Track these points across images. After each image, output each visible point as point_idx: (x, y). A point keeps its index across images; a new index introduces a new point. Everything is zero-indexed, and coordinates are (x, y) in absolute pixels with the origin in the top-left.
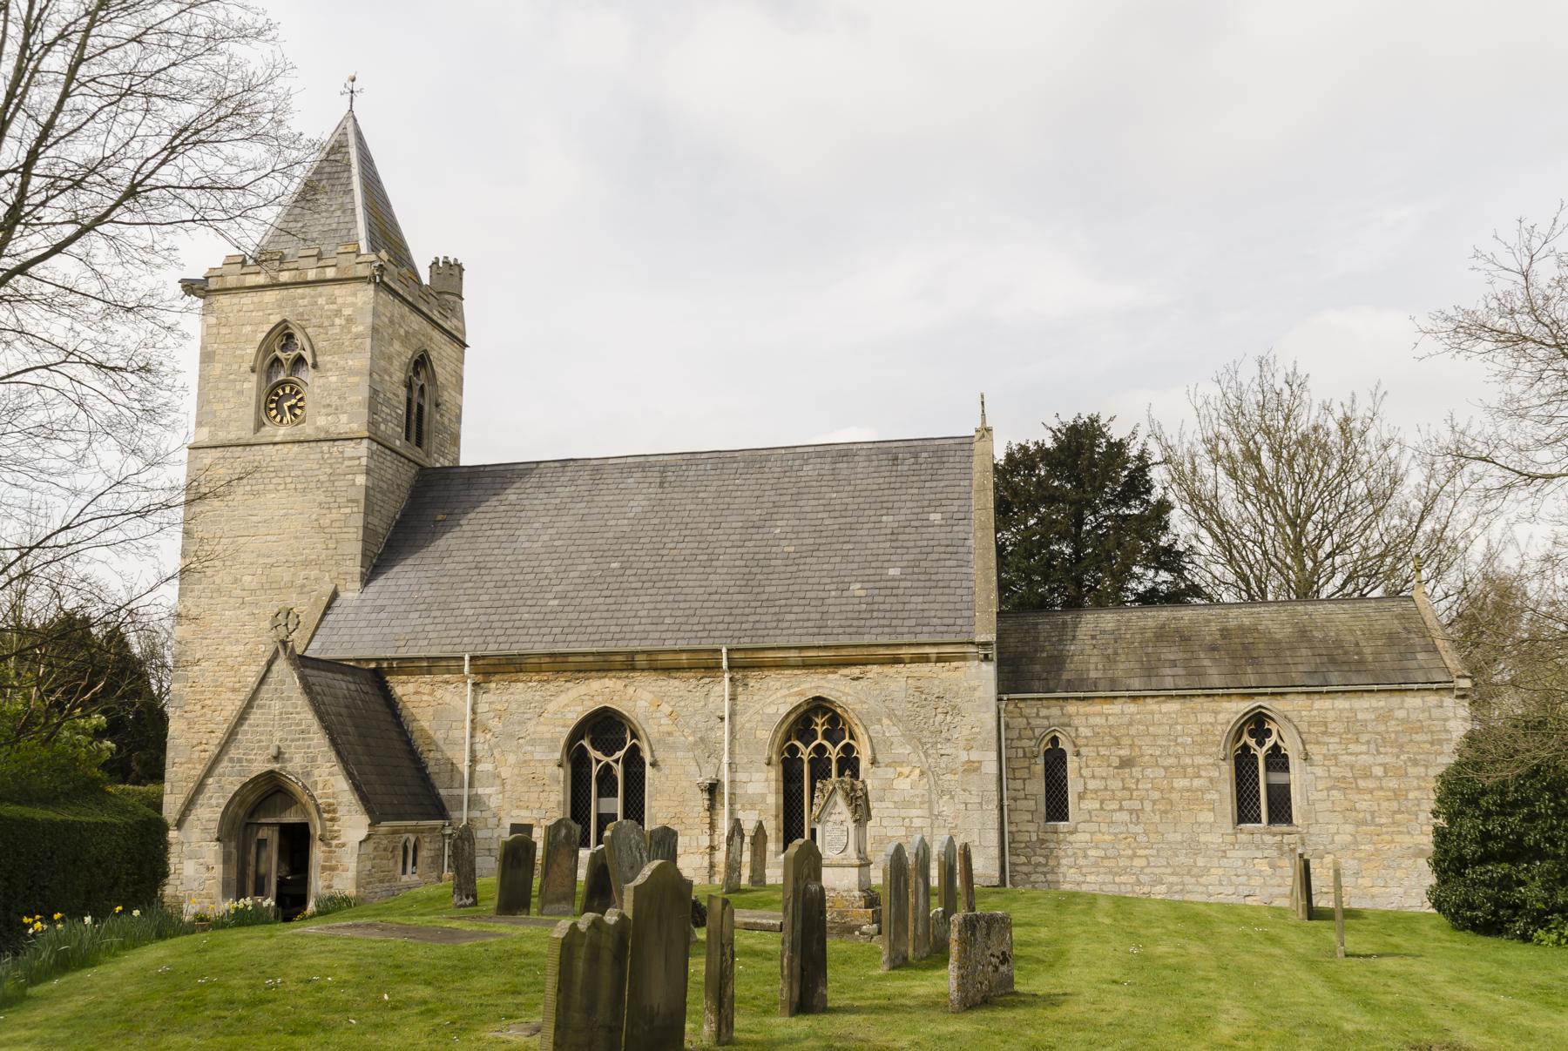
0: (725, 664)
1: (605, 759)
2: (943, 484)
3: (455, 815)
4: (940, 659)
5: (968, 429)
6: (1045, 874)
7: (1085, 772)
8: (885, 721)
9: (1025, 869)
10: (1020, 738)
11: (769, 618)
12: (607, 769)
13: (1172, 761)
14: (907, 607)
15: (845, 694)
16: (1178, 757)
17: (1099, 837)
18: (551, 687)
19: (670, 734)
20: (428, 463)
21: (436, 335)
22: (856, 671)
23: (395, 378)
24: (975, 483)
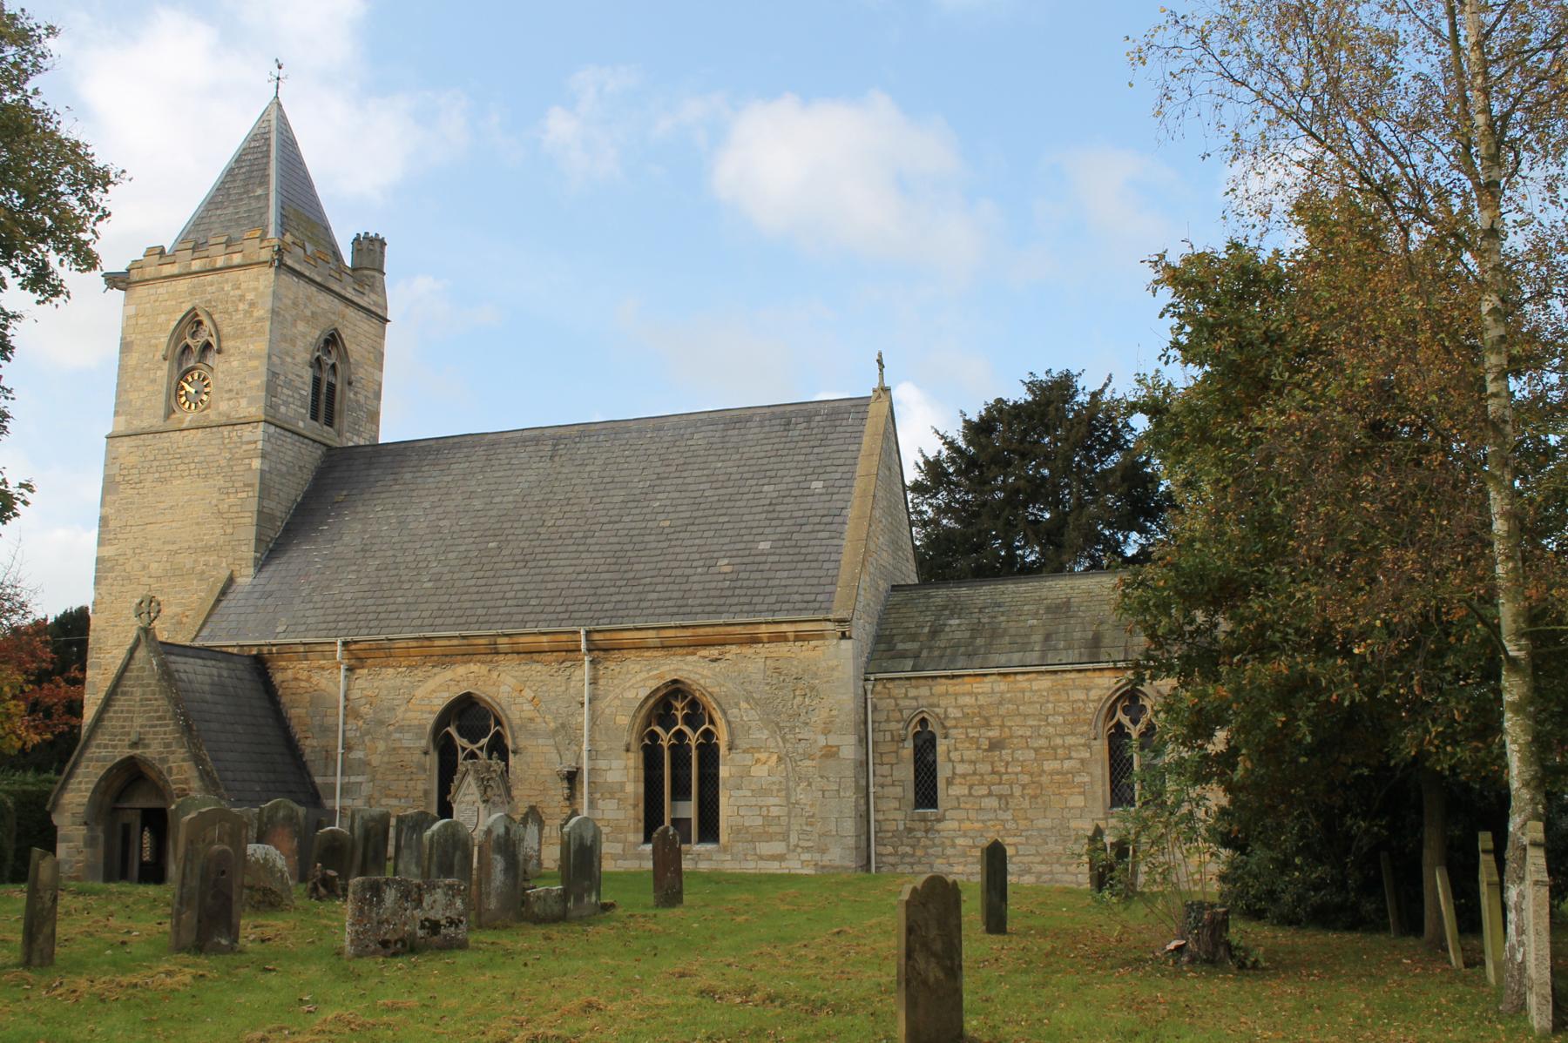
0: (583, 646)
1: (471, 747)
2: (829, 449)
3: (328, 803)
4: (799, 637)
6: (912, 864)
7: (955, 756)
8: (743, 705)
9: (891, 860)
10: (888, 721)
11: (630, 597)
13: (1042, 742)
14: (771, 583)
15: (704, 677)
18: (420, 673)
19: (531, 720)
20: (336, 443)
21: (351, 312)
23: (298, 359)
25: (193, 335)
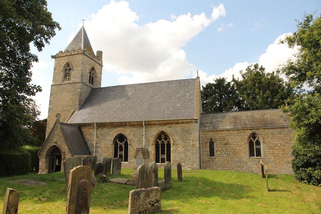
0: (144, 124)
1: (121, 144)
5: (195, 77)
9: (205, 166)
10: (204, 139)
12: (121, 145)
13: (236, 143)
16: (237, 142)
17: (221, 160)
19: (133, 139)
21: (96, 64)
22: (170, 125)
24: (196, 87)
25: (68, 67)
